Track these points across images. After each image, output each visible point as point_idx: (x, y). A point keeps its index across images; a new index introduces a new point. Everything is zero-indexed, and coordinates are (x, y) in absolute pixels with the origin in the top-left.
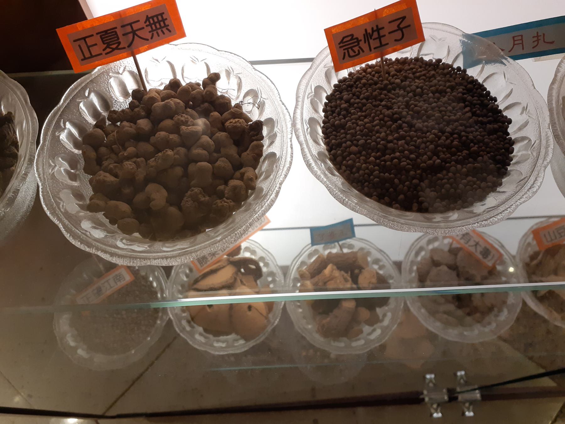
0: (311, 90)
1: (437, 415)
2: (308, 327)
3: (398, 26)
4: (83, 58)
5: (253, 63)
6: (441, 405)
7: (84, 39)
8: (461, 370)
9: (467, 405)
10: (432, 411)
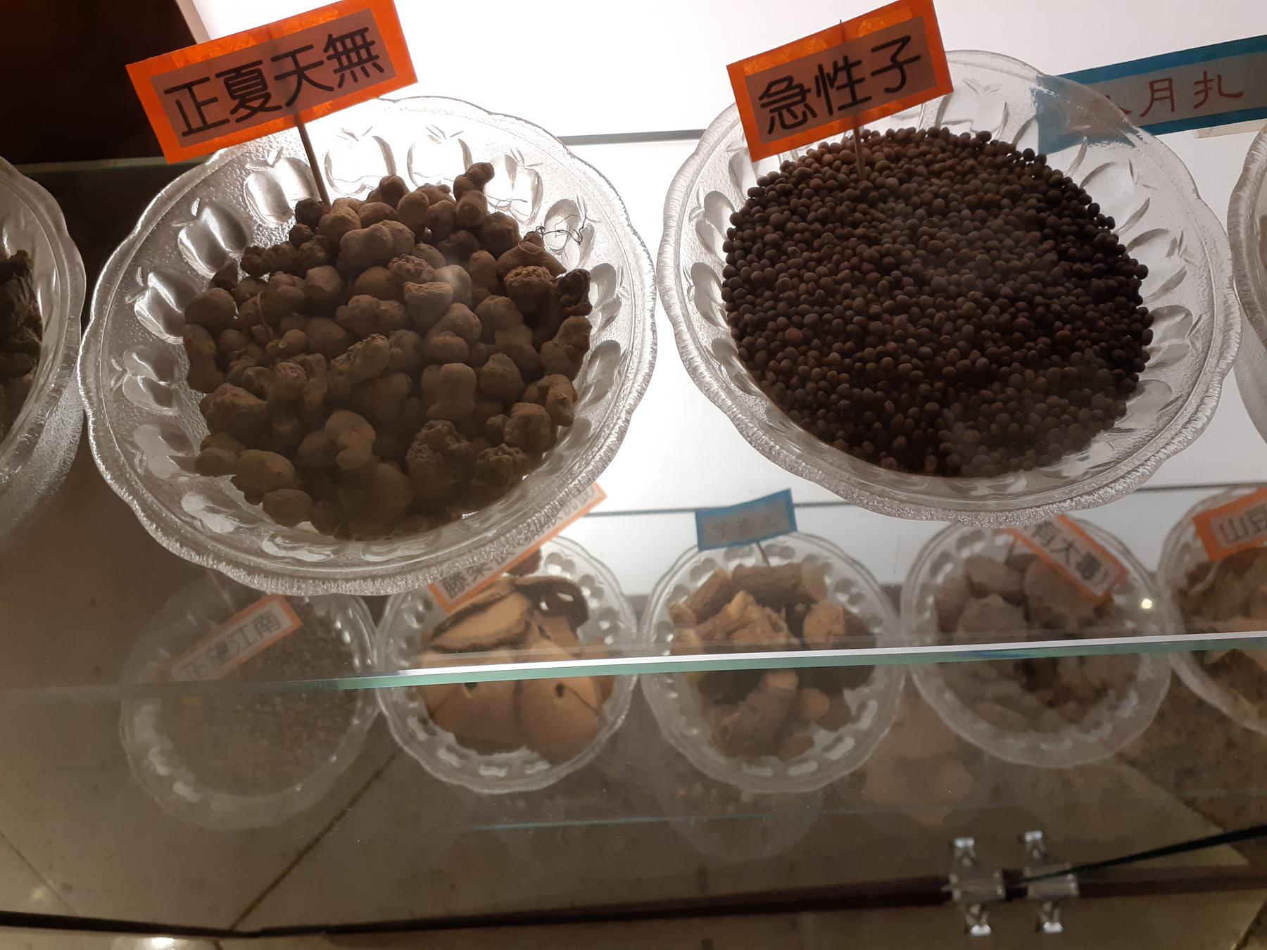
0: (696, 202)
1: (980, 930)
2: (690, 733)
3: (893, 58)
4: (186, 129)
5: (567, 141)
6: (989, 908)
7: (189, 86)
8: (1033, 829)
9: (1047, 907)
10: (970, 920)
